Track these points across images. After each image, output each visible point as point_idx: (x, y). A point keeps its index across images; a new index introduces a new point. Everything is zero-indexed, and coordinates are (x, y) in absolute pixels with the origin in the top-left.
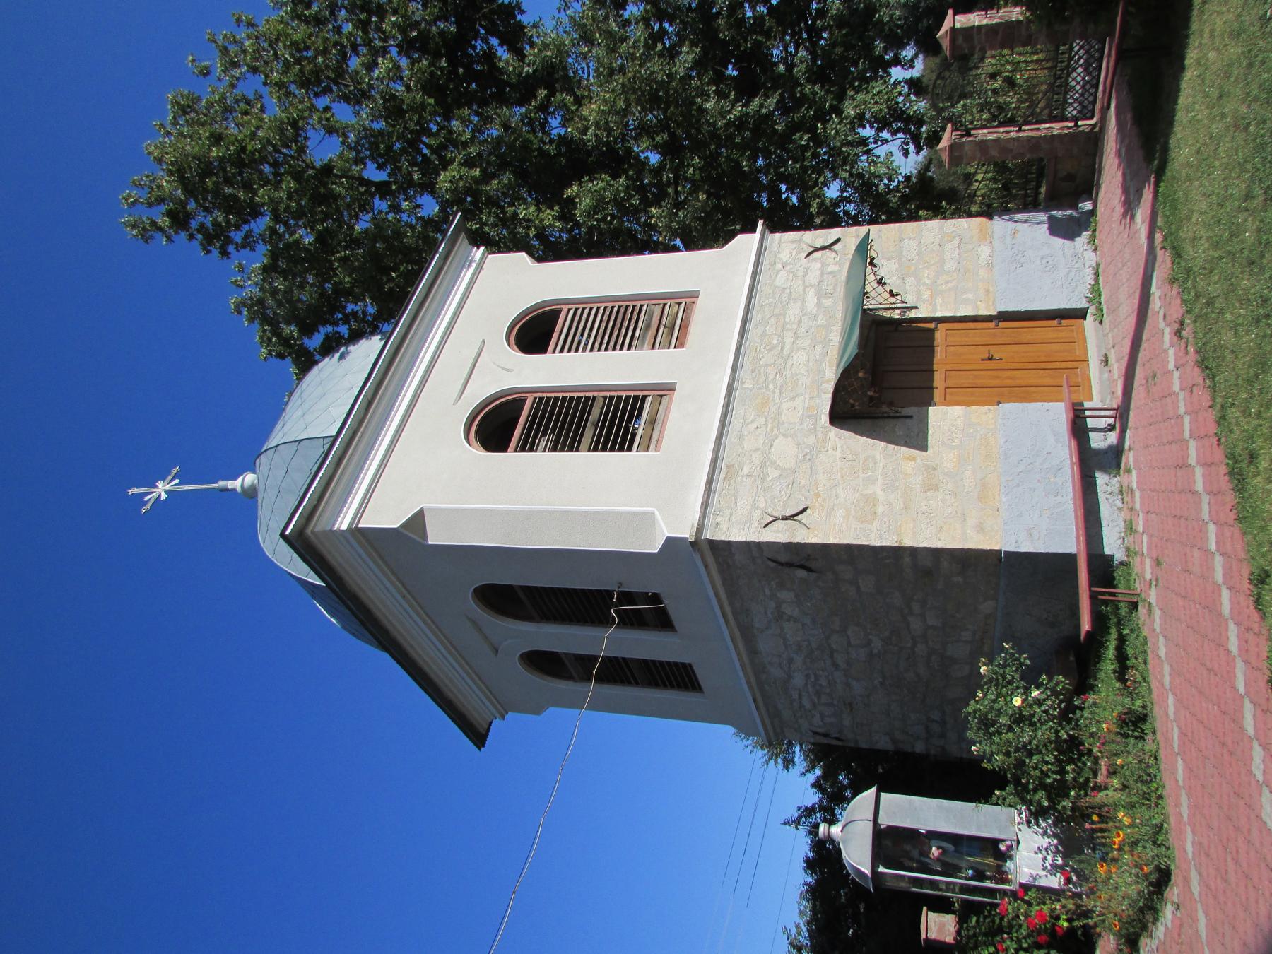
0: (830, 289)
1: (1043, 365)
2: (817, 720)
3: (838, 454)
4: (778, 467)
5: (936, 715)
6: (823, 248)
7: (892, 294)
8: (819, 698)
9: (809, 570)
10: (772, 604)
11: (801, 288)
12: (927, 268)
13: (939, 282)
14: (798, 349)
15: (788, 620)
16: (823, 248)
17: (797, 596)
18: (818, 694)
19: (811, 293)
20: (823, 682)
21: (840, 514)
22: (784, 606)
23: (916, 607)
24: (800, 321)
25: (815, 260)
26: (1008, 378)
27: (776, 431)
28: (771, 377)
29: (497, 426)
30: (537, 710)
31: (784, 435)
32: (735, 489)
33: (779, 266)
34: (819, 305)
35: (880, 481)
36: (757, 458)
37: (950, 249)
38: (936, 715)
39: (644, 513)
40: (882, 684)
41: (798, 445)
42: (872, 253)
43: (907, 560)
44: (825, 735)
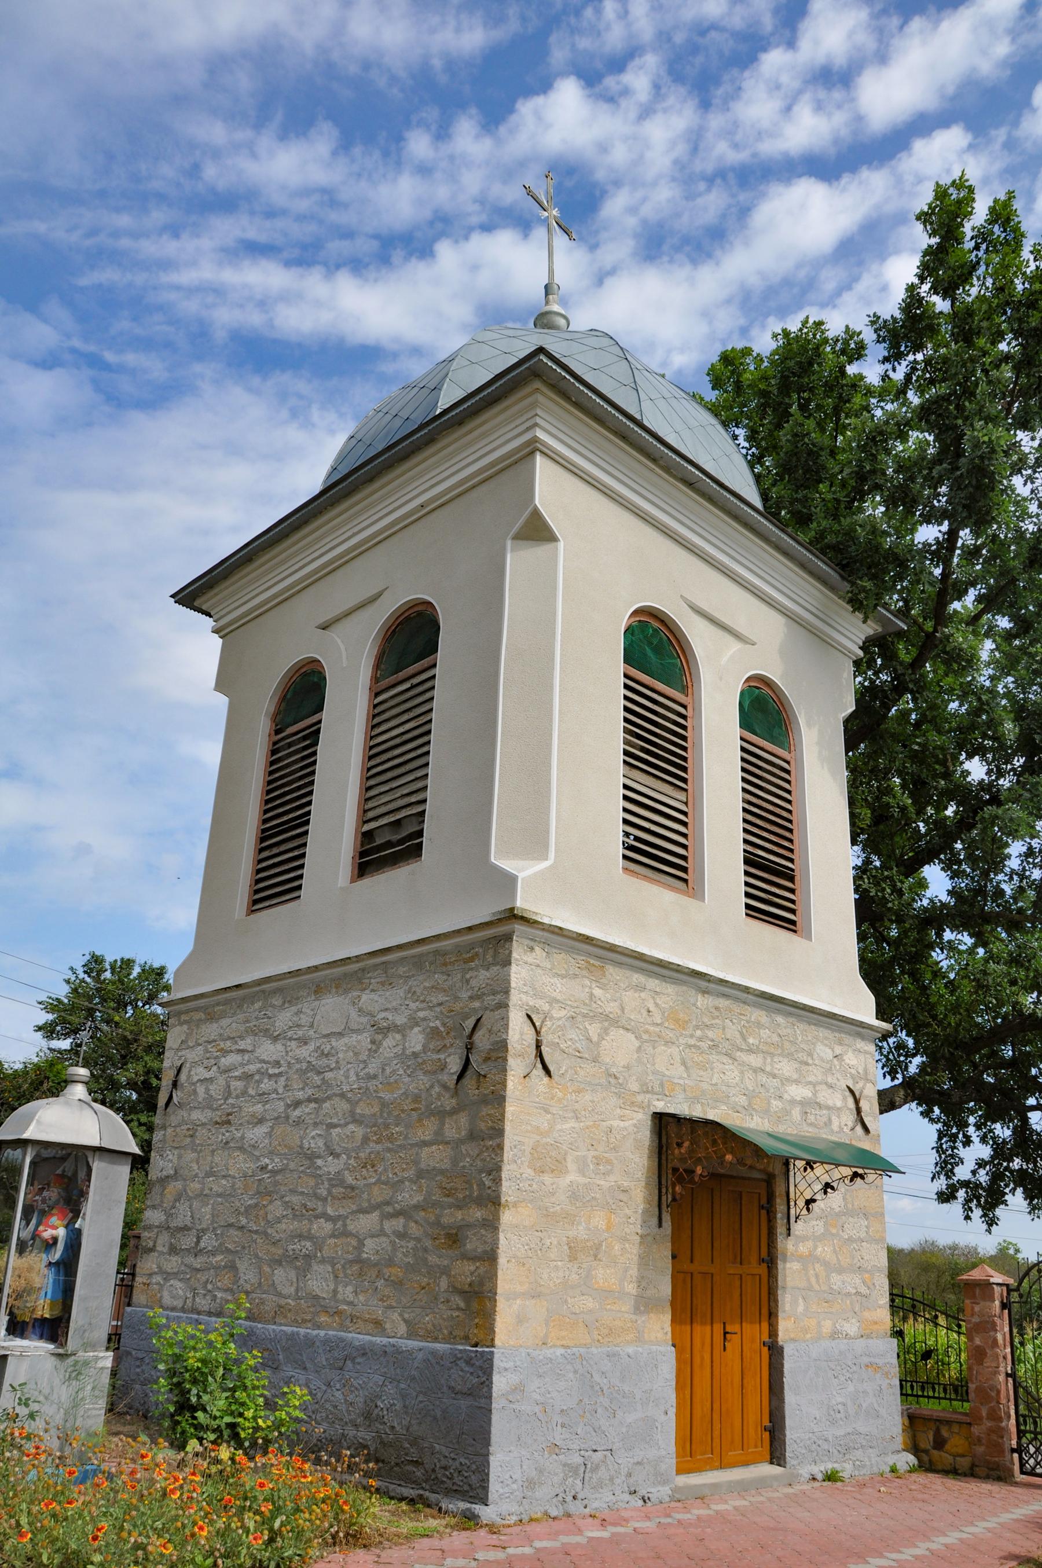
0: (811, 1118)
1: (716, 1406)
2: (200, 1073)
3: (616, 1123)
5: (208, 1241)
6: (859, 1110)
7: (809, 1202)
8: (239, 1078)
9: (461, 1076)
10: (400, 1020)
12: (835, 1251)
13: (817, 1266)
14: (742, 1072)
15: (373, 1042)
16: (859, 1110)
17: (415, 1055)
18: (247, 1077)
19: (806, 1092)
20: (266, 1085)
21: (543, 1121)
22: (398, 1037)
23: (398, 1223)
24: (774, 1076)
25: (845, 1098)
26: (702, 1358)
27: (645, 1037)
28: (710, 1034)
29: (655, 648)
31: (640, 1047)
33: (838, 1050)
34: (793, 1102)
35: (582, 1180)
36: (612, 1008)
37: (853, 1282)
38: (208, 1241)
39: (546, 846)
40: (263, 1168)
41: (628, 1067)
42: (871, 1177)
43: (478, 1214)
44: (175, 1084)
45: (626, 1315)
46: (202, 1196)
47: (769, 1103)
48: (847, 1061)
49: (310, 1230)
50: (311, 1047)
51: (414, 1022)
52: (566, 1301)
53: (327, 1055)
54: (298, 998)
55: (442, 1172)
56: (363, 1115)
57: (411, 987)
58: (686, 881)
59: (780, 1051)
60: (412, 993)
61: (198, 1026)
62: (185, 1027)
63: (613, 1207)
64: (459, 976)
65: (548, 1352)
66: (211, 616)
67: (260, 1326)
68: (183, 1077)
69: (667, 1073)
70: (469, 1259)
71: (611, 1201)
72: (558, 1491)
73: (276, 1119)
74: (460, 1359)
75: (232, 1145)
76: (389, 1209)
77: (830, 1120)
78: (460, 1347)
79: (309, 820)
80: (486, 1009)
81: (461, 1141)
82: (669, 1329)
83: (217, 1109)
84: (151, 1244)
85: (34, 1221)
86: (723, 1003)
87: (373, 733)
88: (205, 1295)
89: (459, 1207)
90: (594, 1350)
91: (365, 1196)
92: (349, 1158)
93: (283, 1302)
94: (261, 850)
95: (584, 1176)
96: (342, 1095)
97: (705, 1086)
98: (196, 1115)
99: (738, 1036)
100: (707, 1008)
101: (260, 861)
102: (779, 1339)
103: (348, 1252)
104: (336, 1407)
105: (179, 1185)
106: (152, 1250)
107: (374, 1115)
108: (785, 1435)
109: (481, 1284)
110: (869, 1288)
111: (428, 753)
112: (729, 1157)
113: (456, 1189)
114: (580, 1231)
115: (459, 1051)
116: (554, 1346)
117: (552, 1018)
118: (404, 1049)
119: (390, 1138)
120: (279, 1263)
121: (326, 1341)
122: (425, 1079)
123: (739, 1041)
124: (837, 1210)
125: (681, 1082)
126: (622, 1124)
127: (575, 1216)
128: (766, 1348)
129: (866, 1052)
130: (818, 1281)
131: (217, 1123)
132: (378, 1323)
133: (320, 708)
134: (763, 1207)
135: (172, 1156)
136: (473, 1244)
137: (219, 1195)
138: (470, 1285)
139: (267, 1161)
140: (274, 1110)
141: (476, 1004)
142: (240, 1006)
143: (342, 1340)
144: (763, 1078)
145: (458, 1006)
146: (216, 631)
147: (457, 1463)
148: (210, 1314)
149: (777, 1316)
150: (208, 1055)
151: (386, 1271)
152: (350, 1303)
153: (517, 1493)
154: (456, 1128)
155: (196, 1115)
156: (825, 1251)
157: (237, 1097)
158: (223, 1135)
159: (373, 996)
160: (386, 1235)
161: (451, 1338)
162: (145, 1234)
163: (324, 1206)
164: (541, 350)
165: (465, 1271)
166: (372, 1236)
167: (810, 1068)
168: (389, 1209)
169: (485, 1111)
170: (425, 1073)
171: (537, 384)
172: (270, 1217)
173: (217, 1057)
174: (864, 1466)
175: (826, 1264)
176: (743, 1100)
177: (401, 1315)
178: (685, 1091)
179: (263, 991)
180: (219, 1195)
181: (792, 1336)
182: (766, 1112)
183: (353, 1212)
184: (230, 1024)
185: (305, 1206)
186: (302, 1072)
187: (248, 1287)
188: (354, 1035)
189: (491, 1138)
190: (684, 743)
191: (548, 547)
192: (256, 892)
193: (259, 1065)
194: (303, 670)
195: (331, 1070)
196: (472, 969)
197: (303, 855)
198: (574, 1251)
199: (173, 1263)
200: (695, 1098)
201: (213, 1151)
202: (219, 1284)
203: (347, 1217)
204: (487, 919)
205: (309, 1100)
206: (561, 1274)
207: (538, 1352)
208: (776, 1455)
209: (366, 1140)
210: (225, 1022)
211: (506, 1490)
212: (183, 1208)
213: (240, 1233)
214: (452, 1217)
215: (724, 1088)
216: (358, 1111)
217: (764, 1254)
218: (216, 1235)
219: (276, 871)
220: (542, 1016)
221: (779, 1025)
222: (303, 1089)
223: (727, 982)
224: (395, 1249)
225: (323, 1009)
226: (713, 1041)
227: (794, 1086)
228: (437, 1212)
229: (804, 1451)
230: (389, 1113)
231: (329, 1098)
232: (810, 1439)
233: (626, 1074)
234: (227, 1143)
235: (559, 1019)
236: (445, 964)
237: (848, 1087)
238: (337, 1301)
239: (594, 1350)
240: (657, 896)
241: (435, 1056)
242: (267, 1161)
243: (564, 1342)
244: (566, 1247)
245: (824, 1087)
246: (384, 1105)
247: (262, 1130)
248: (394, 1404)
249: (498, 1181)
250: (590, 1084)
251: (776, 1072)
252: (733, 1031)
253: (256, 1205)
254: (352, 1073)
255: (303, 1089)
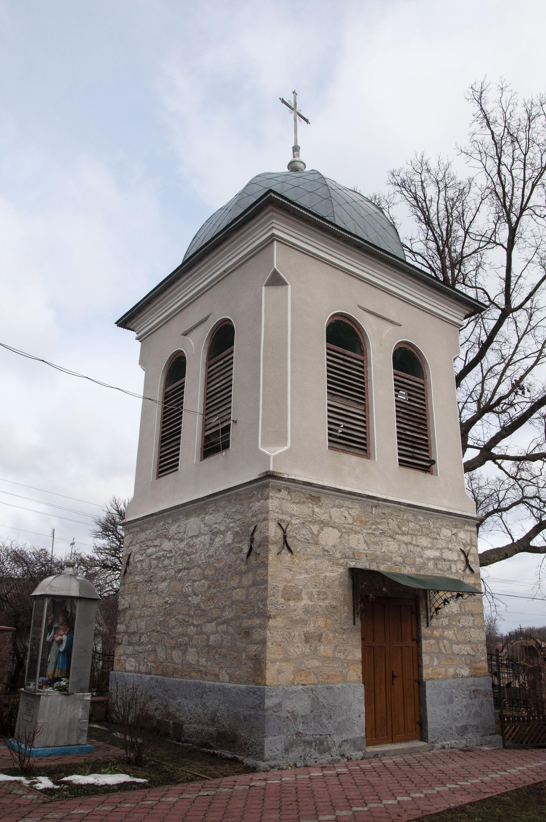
0: (440, 566)
1: (389, 713)
2: (139, 557)
3: (328, 574)
4: (319, 532)
5: (144, 639)
6: (467, 561)
7: (437, 609)
8: (154, 559)
9: (249, 554)
10: (222, 528)
11: (439, 546)
12: (455, 633)
13: (445, 641)
14: (399, 545)
15: (211, 539)
18: (158, 558)
19: (437, 554)
20: (166, 562)
21: (288, 575)
22: (222, 536)
23: (224, 627)
24: (418, 546)
25: (459, 555)
27: (344, 530)
29: (344, 335)
30: (142, 362)
31: (341, 536)
32: (304, 503)
34: (429, 559)
35: (310, 603)
38: (144, 639)
40: (166, 602)
41: (334, 546)
43: (258, 621)
45: (337, 669)
46: (140, 617)
47: (415, 560)
48: (460, 536)
49: (187, 631)
50: (185, 543)
51: (228, 529)
52: (304, 663)
53: (192, 547)
54: (178, 519)
55: (242, 602)
56: (207, 575)
57: (226, 512)
58: (365, 450)
59: (421, 533)
60: (227, 516)
61: (137, 535)
62: (131, 535)
63: (328, 616)
64: (247, 505)
65: (295, 688)
66: (134, 331)
67: (167, 678)
68: (131, 560)
69: (356, 548)
70: (254, 644)
71: (327, 613)
72: (301, 754)
73: (171, 578)
74: (251, 691)
75: (153, 592)
76: (220, 620)
77: (450, 567)
78: (251, 686)
79: (181, 432)
80: (259, 521)
81: (249, 587)
82: (361, 675)
83: (146, 575)
84: (120, 641)
85: (53, 633)
86: (387, 511)
87: (208, 387)
88: (144, 664)
89: (249, 619)
90: (320, 686)
91: (209, 614)
92: (202, 596)
93: (176, 667)
94: (162, 447)
95: (311, 601)
96: (199, 566)
97: (378, 553)
98: (137, 578)
99: (397, 527)
100: (378, 514)
101: (161, 452)
102: (424, 678)
103: (203, 642)
104: (199, 716)
105: (131, 612)
106: (120, 644)
107: (212, 575)
108: (427, 726)
109: (259, 655)
110: (475, 652)
111: (231, 396)
112: (384, 589)
113: (248, 610)
114: (311, 628)
115: (248, 542)
116: (298, 684)
117: (292, 524)
118: (224, 542)
119: (219, 586)
120: (174, 648)
121: (195, 685)
122: (234, 557)
123: (397, 530)
124: (456, 612)
125: (365, 552)
126: (332, 574)
127: (307, 621)
128: (417, 683)
129: (471, 531)
130: (445, 649)
131: (146, 581)
132: (216, 676)
133: (184, 376)
134: (413, 613)
135: (127, 598)
136: (256, 636)
137: (148, 616)
138: (255, 656)
139: (168, 599)
140: (170, 574)
141: (255, 519)
142: (154, 524)
143: (201, 684)
144: (411, 548)
145: (246, 520)
146: (138, 339)
147: (251, 741)
148: (146, 673)
149: (422, 667)
150: (141, 548)
151: (219, 650)
152: (204, 666)
153: (280, 756)
154: (247, 580)
155: (137, 578)
156: (449, 634)
157: (154, 568)
158: (149, 586)
159: (211, 517)
160: (218, 633)
161: (247, 682)
162: (118, 636)
163: (192, 620)
164: (271, 191)
165: (253, 649)
166: (213, 634)
167: (439, 541)
168: (220, 620)
169: (260, 571)
170: (234, 553)
171: (271, 207)
172: (170, 626)
173: (145, 549)
174: (473, 742)
175: (450, 641)
176: (400, 559)
177: (226, 671)
178: (367, 556)
179: (164, 516)
180: (148, 616)
181: (431, 677)
182: (414, 564)
183: (205, 622)
184: (150, 533)
185: (184, 620)
186: (182, 555)
187: (161, 660)
188: (203, 536)
189: (262, 585)
190: (362, 381)
191: (282, 288)
192: (160, 467)
193: (163, 553)
194: (177, 356)
195: (194, 554)
196: (252, 502)
197: (179, 449)
198: (307, 638)
199: (130, 650)
200: (372, 559)
201: (145, 595)
202: (150, 659)
203: (202, 625)
204: (257, 477)
205: (185, 569)
206: (300, 649)
207: (289, 688)
208: (422, 735)
209: (209, 587)
210: (148, 532)
211: (274, 754)
212: (133, 622)
213: (157, 634)
214: (247, 623)
215: (389, 554)
216: (206, 573)
217: (415, 636)
218: (147, 635)
219: (166, 457)
220: (286, 523)
221: (420, 520)
222: (182, 563)
223: (388, 500)
224: (222, 640)
225: (189, 524)
226: (382, 530)
227: (429, 551)
228: (240, 621)
229: (438, 734)
230: (219, 574)
231: (193, 567)
232: (441, 728)
233: (334, 550)
234: (151, 591)
235: (296, 524)
236: (241, 500)
237: (461, 550)
238: (199, 665)
239: (320, 686)
240: (350, 461)
241: (238, 545)
242: (168, 599)
243: (304, 683)
244: (303, 636)
245: (447, 550)
246: (216, 570)
247: (165, 584)
248: (224, 714)
249: (265, 605)
250: (313, 555)
251: (419, 544)
252: (393, 524)
253: (164, 620)
254: (203, 555)
255: (182, 563)
